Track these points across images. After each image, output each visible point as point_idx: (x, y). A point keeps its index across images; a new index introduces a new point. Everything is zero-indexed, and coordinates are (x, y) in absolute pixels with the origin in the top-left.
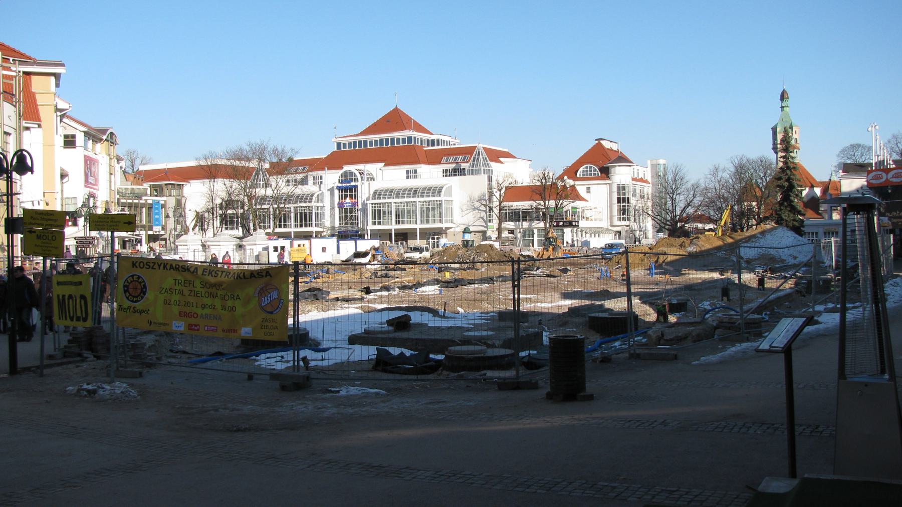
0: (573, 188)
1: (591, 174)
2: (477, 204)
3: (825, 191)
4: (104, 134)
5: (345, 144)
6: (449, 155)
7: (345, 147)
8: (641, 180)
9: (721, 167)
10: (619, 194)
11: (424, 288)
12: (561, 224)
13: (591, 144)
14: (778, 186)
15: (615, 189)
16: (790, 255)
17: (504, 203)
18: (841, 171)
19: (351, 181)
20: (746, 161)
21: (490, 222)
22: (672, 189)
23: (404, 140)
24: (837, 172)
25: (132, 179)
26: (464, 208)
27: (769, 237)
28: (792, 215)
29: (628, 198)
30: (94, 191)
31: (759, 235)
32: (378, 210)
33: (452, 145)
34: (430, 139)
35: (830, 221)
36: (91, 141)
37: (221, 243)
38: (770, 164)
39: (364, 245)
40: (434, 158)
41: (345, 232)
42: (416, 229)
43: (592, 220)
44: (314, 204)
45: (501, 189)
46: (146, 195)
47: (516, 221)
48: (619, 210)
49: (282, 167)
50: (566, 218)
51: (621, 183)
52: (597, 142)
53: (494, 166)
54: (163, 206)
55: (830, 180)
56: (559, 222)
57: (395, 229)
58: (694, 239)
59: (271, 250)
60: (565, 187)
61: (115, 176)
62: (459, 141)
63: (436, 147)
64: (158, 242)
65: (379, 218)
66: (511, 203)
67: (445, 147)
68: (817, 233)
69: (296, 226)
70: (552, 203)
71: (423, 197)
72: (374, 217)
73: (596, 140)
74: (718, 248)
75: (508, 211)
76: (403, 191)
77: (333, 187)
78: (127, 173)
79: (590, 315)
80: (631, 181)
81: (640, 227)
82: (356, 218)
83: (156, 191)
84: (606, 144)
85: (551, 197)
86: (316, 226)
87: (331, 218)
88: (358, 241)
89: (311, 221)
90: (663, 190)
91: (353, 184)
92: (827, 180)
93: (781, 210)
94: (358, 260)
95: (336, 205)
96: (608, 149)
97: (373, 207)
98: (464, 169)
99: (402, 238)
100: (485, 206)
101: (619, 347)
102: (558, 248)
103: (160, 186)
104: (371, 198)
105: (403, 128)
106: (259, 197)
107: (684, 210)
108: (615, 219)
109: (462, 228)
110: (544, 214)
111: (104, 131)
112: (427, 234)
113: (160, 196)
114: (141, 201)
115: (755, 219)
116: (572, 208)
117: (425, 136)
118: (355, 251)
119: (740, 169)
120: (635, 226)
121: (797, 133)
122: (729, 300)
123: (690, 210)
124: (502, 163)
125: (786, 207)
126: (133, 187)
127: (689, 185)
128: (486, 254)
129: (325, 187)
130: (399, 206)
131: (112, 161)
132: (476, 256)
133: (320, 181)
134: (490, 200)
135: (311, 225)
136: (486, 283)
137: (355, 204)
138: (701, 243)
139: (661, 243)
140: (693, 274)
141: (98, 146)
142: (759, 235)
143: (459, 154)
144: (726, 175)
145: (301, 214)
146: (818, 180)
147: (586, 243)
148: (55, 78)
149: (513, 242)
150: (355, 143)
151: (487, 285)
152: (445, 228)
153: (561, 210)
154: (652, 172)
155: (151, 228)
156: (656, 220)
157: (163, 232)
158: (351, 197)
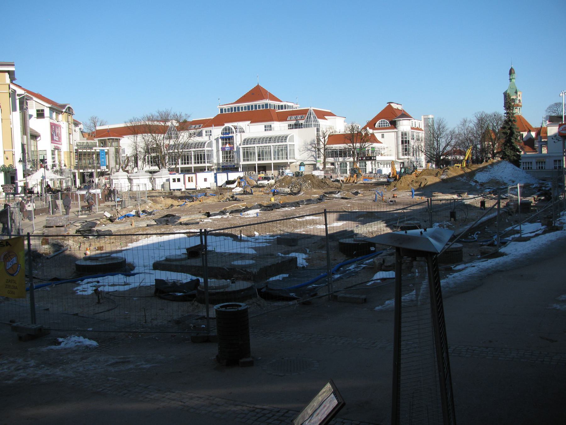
0: (373, 135)
1: (384, 126)
2: (310, 147)
3: (538, 134)
4: (64, 108)
5: (225, 110)
6: (291, 115)
7: (225, 111)
8: (418, 129)
9: (468, 119)
10: (402, 138)
11: (249, 212)
12: (364, 158)
13: (385, 105)
14: (504, 133)
15: (400, 135)
16: (510, 180)
17: (327, 146)
18: (548, 121)
19: (229, 133)
20: (484, 115)
21: (319, 158)
22: (437, 134)
23: (263, 106)
24: (545, 121)
25: (87, 136)
26: (302, 149)
27: (496, 167)
28: (513, 152)
29: (408, 141)
30: (58, 145)
31: (489, 167)
32: (247, 151)
33: (294, 108)
34: (280, 105)
35: (541, 155)
36: (55, 113)
37: (140, 177)
38: (501, 117)
39: (233, 176)
40: (282, 117)
41: (226, 166)
42: (271, 163)
43: (385, 155)
44: (206, 149)
45: (325, 137)
46: (96, 146)
47: (344, 157)
48: (403, 149)
49: (184, 126)
50: (367, 155)
51: (404, 131)
52: (388, 104)
53: (321, 121)
54: (107, 153)
55: (542, 126)
56: (362, 157)
57: (258, 164)
58: (445, 170)
59: (171, 181)
60: (367, 134)
61: (72, 135)
62: (299, 106)
63: (284, 110)
64: (104, 177)
65: (248, 156)
66: (331, 146)
67: (290, 110)
68: (531, 163)
69: (195, 163)
70: (358, 145)
71: (275, 142)
72: (244, 156)
73: (387, 103)
74: (461, 176)
75: (330, 151)
76: (262, 139)
77: (218, 137)
78: (84, 132)
79: (342, 241)
80: (410, 129)
81: (417, 159)
82: (233, 157)
83: (102, 143)
84: (394, 106)
85: (357, 141)
86: (207, 163)
87: (217, 158)
88: (229, 174)
89: (205, 160)
90: (432, 135)
91: (230, 135)
92: (540, 127)
93: (505, 148)
94: (229, 186)
95: (220, 149)
96: (395, 109)
97: (243, 150)
98: (302, 124)
99: (263, 169)
100: (315, 148)
101: (354, 269)
102: (360, 175)
103: (105, 140)
104: (242, 144)
105: (262, 98)
106: (171, 145)
107: (444, 148)
108: (400, 154)
109: (299, 163)
110: (353, 152)
111: (63, 106)
112: (278, 167)
113: (105, 147)
114: (92, 151)
115: (491, 154)
116: (372, 148)
117: (277, 103)
118: (226, 180)
119: (481, 121)
120: (413, 159)
121: (520, 96)
122: (455, 220)
123: (449, 148)
124: (327, 119)
125: (509, 147)
126: (88, 141)
127: (448, 132)
128: (309, 181)
129: (213, 138)
130: (260, 149)
131: (71, 125)
132: (303, 183)
133: (210, 133)
134: (318, 144)
135: (205, 162)
136: (293, 207)
137: (232, 148)
138: (449, 172)
139: (424, 173)
140: (440, 196)
141: (60, 116)
142: (489, 167)
143: (299, 114)
144: (472, 125)
145: (198, 155)
146: (534, 126)
147: (380, 171)
148: (9, 74)
149: (333, 170)
150: (232, 108)
151: (294, 208)
152: (290, 162)
153: (364, 149)
154: (424, 123)
155: (99, 168)
156: (427, 154)
157: (107, 170)
158: (230, 144)
